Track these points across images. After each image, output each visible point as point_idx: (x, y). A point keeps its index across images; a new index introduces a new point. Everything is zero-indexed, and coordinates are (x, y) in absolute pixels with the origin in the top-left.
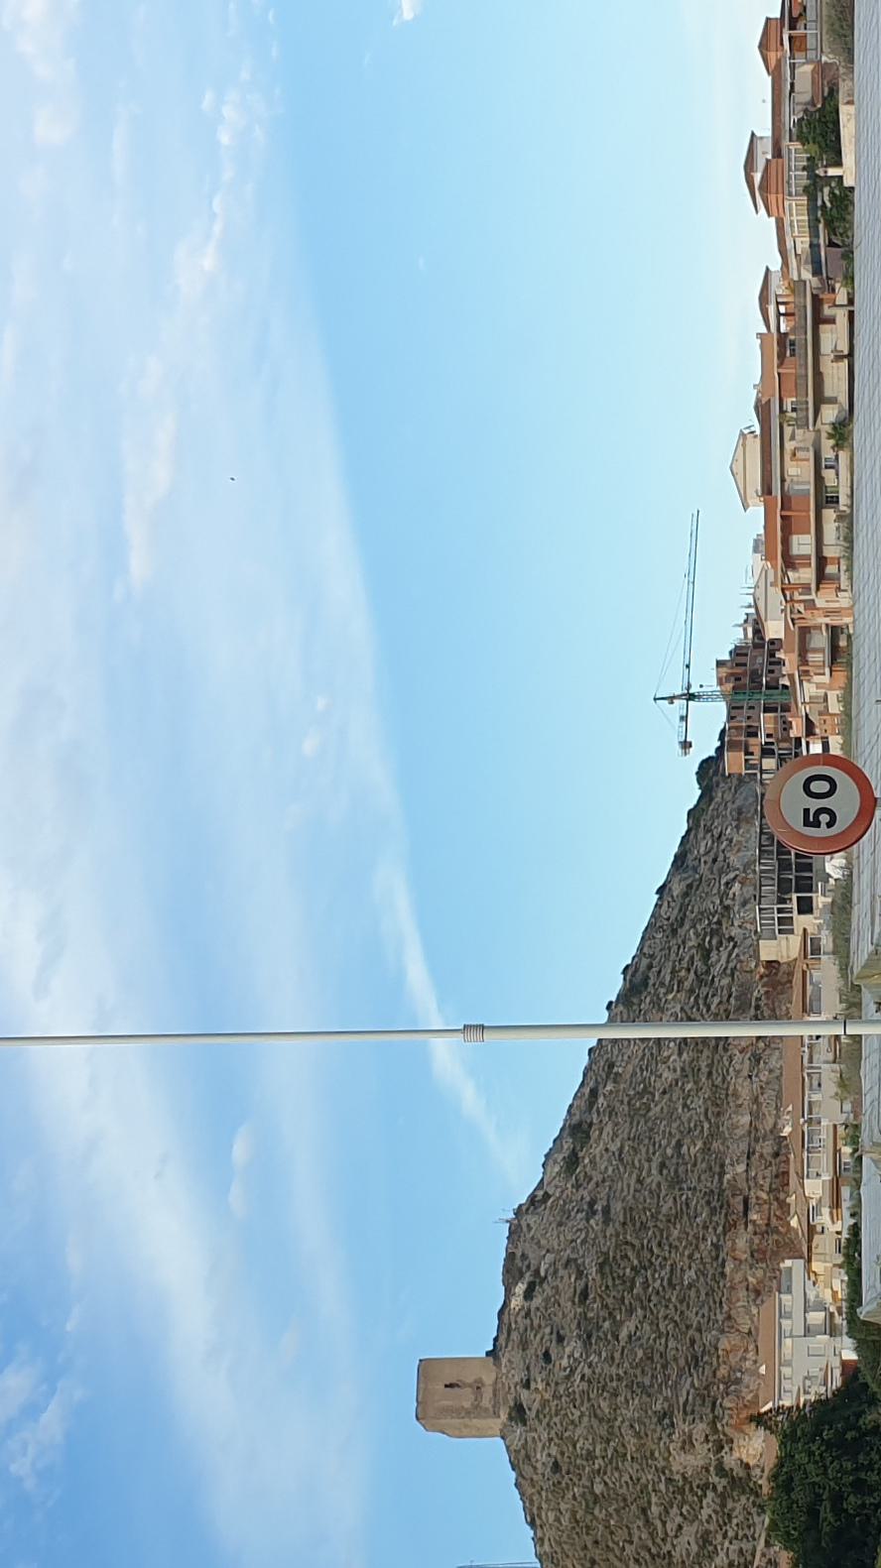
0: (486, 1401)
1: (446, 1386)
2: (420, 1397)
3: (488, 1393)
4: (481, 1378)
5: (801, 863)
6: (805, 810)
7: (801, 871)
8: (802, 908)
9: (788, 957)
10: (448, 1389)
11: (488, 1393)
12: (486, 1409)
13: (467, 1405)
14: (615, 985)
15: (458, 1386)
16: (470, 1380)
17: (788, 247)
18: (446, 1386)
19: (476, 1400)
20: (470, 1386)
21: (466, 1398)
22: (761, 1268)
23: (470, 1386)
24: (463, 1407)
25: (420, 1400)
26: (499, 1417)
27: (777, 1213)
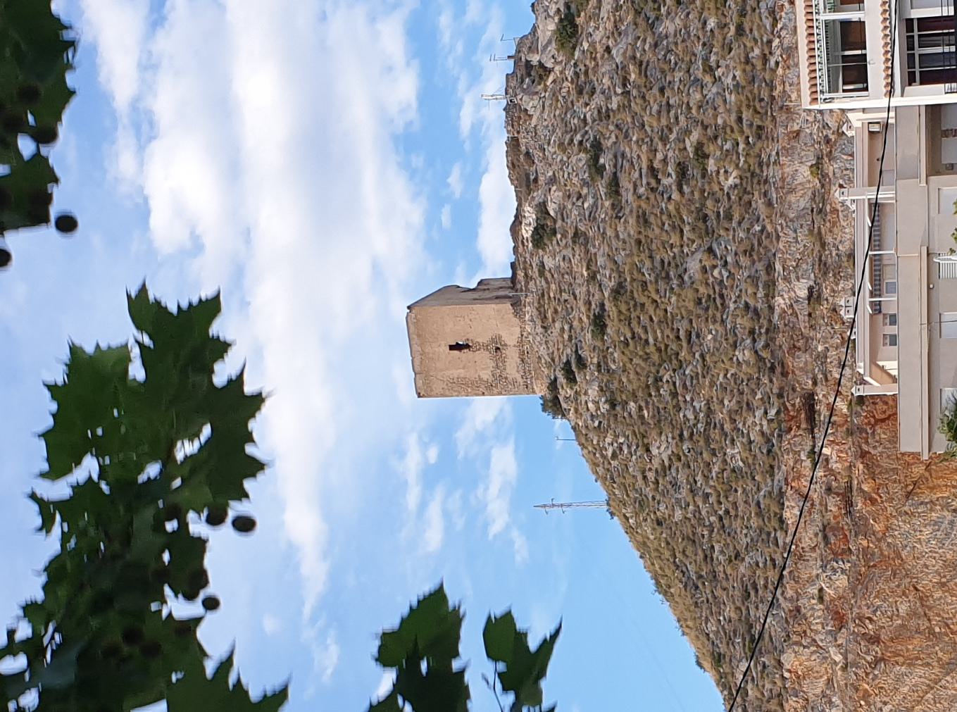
0: (512, 368)
1: (452, 348)
2: (417, 362)
3: (512, 356)
4: (500, 337)
5: (861, 49)
6: (450, 349)
7: (862, 55)
8: (924, 57)
9: (833, 448)
10: (456, 352)
11: (512, 356)
12: (515, 382)
13: (486, 375)
14: (44, 411)
15: (467, 346)
16: (483, 339)
17: (953, 8)
18: (452, 348)
19: (497, 367)
20: (486, 347)
21: (481, 365)
22: (843, 571)
23: (486, 347)
24: (481, 379)
25: (418, 385)
26: (534, 392)
27: (865, 487)
